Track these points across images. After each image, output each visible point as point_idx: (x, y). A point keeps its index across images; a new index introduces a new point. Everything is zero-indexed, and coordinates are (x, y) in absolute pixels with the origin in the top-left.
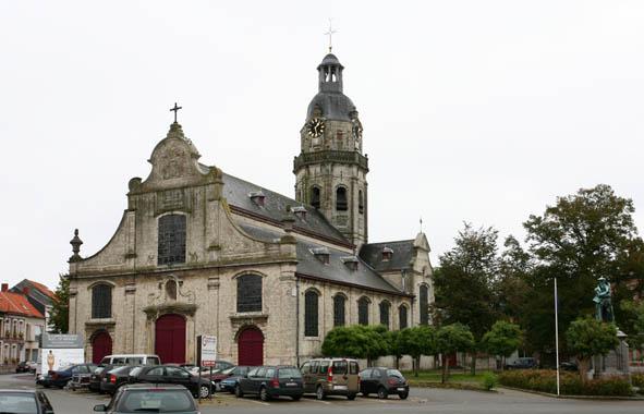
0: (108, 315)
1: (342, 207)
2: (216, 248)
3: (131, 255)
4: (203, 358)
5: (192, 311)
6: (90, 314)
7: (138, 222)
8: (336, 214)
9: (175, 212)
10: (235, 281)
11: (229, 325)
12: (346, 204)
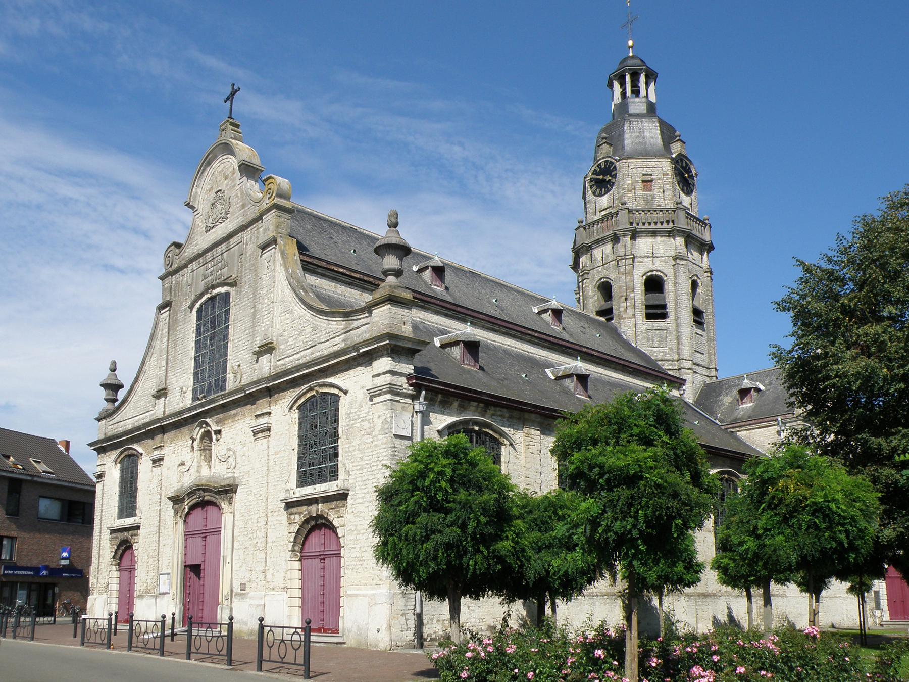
0: (133, 514)
1: (656, 312)
2: (267, 348)
3: (161, 393)
4: (426, 631)
5: (228, 490)
6: (115, 511)
7: (172, 326)
8: (644, 325)
9: (215, 292)
10: (295, 415)
11: (284, 516)
12: (664, 307)
